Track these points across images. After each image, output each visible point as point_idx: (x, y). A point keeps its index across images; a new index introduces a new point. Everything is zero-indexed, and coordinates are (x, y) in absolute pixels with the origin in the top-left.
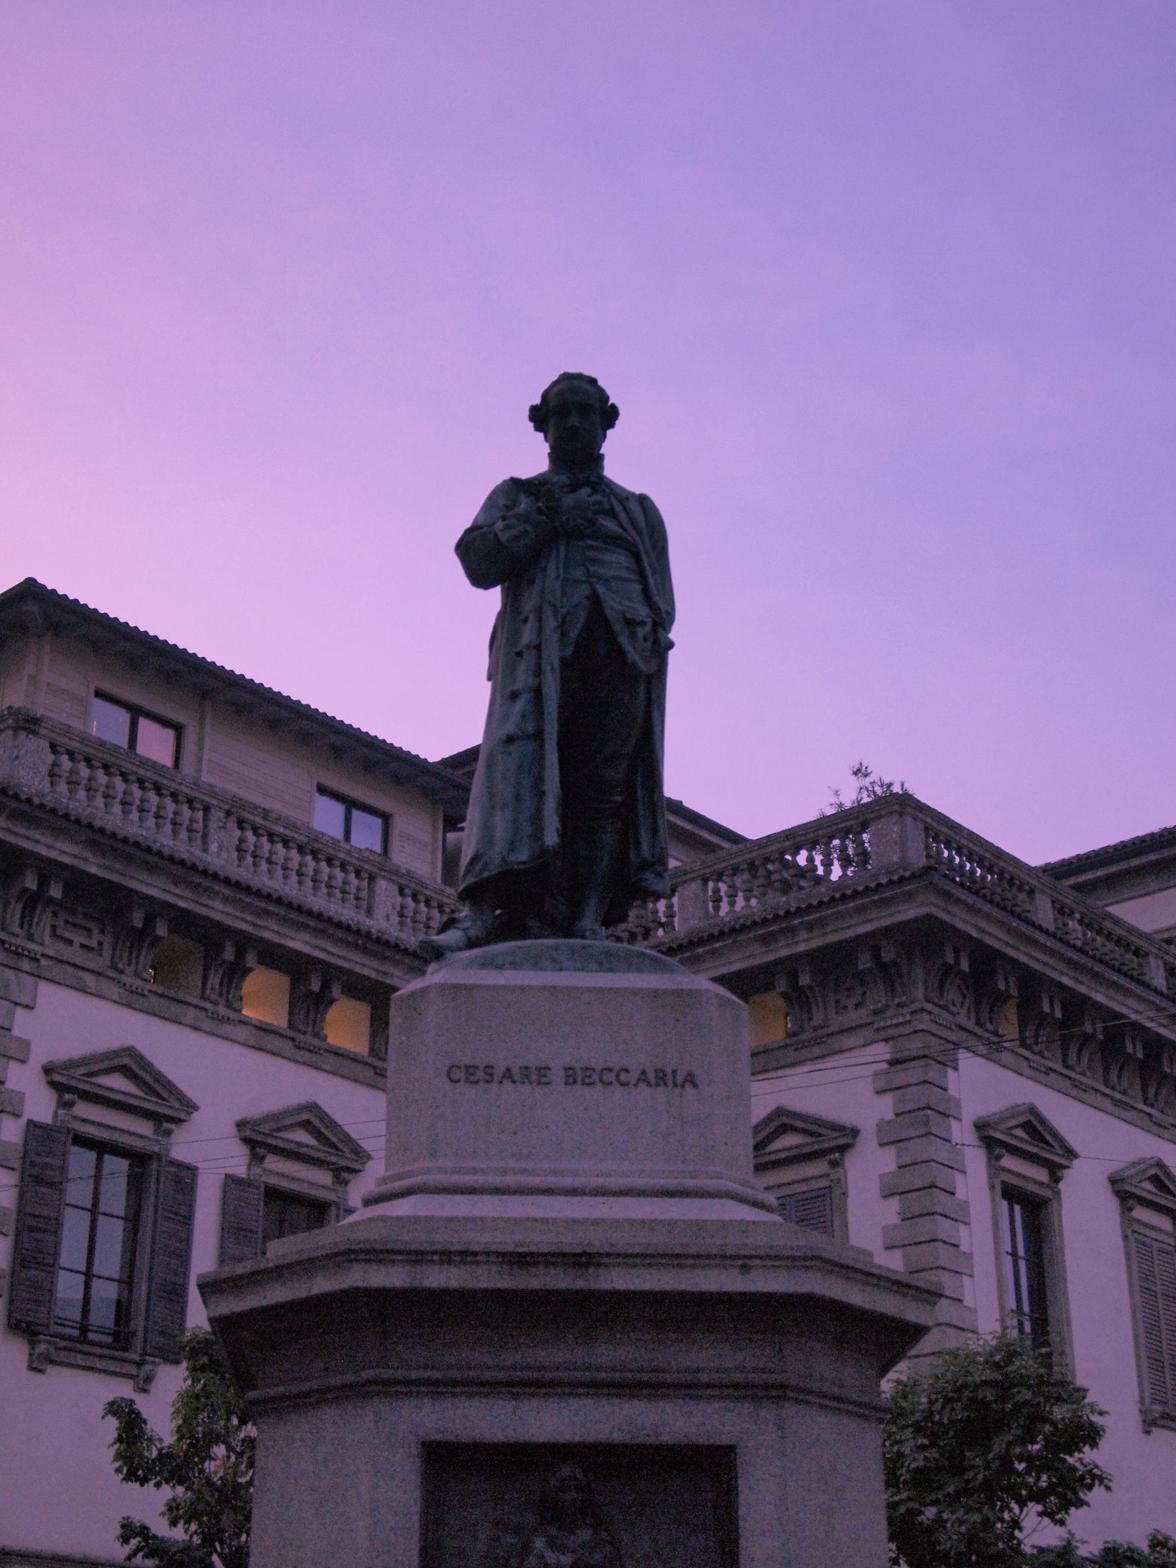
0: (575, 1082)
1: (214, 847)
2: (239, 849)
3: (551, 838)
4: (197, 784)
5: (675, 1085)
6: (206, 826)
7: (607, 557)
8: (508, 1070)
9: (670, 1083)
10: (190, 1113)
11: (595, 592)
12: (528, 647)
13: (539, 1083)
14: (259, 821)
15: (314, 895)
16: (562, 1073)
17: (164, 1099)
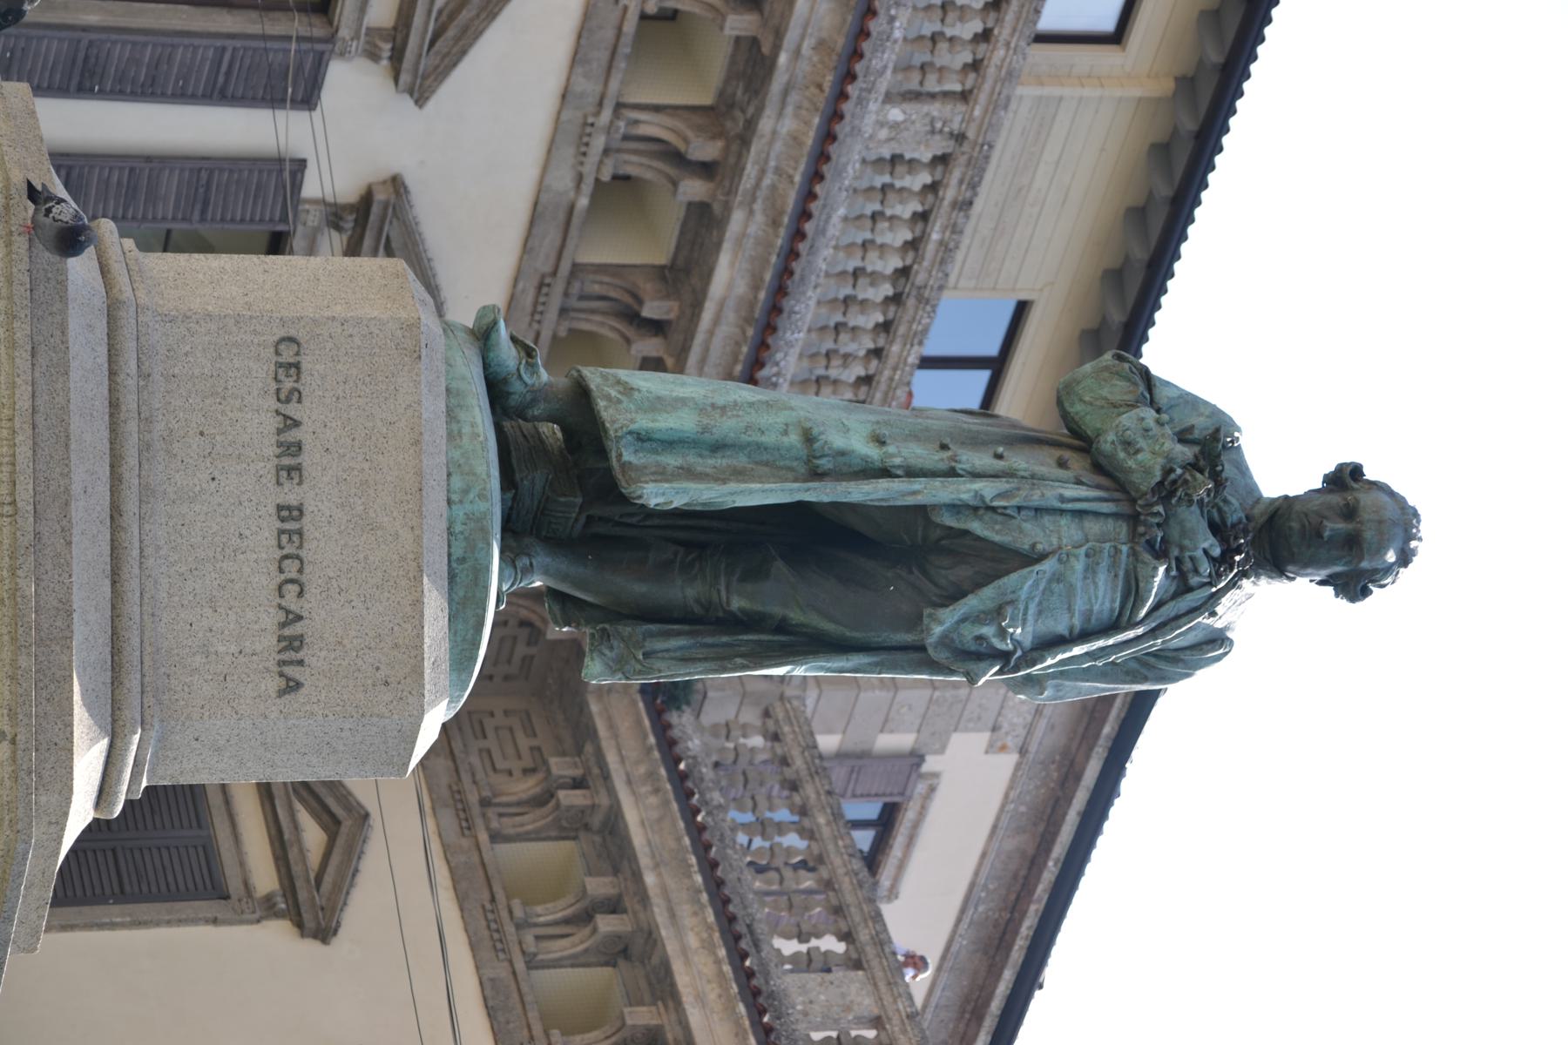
0: (283, 520)
1: (895, 114)
2: (896, 159)
3: (656, 495)
4: (1011, 76)
5: (282, 663)
6: (933, 96)
7: (1102, 577)
8: (297, 424)
9: (286, 656)
10: (411, 93)
11: (1042, 557)
12: (953, 459)
13: (279, 468)
14: (949, 194)
15: (819, 303)
16: (292, 500)
17: (432, 43)
